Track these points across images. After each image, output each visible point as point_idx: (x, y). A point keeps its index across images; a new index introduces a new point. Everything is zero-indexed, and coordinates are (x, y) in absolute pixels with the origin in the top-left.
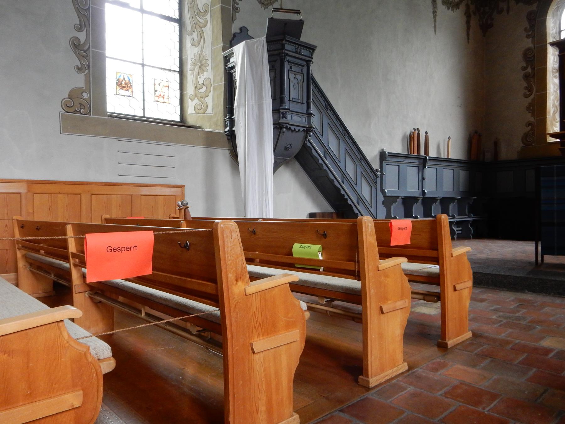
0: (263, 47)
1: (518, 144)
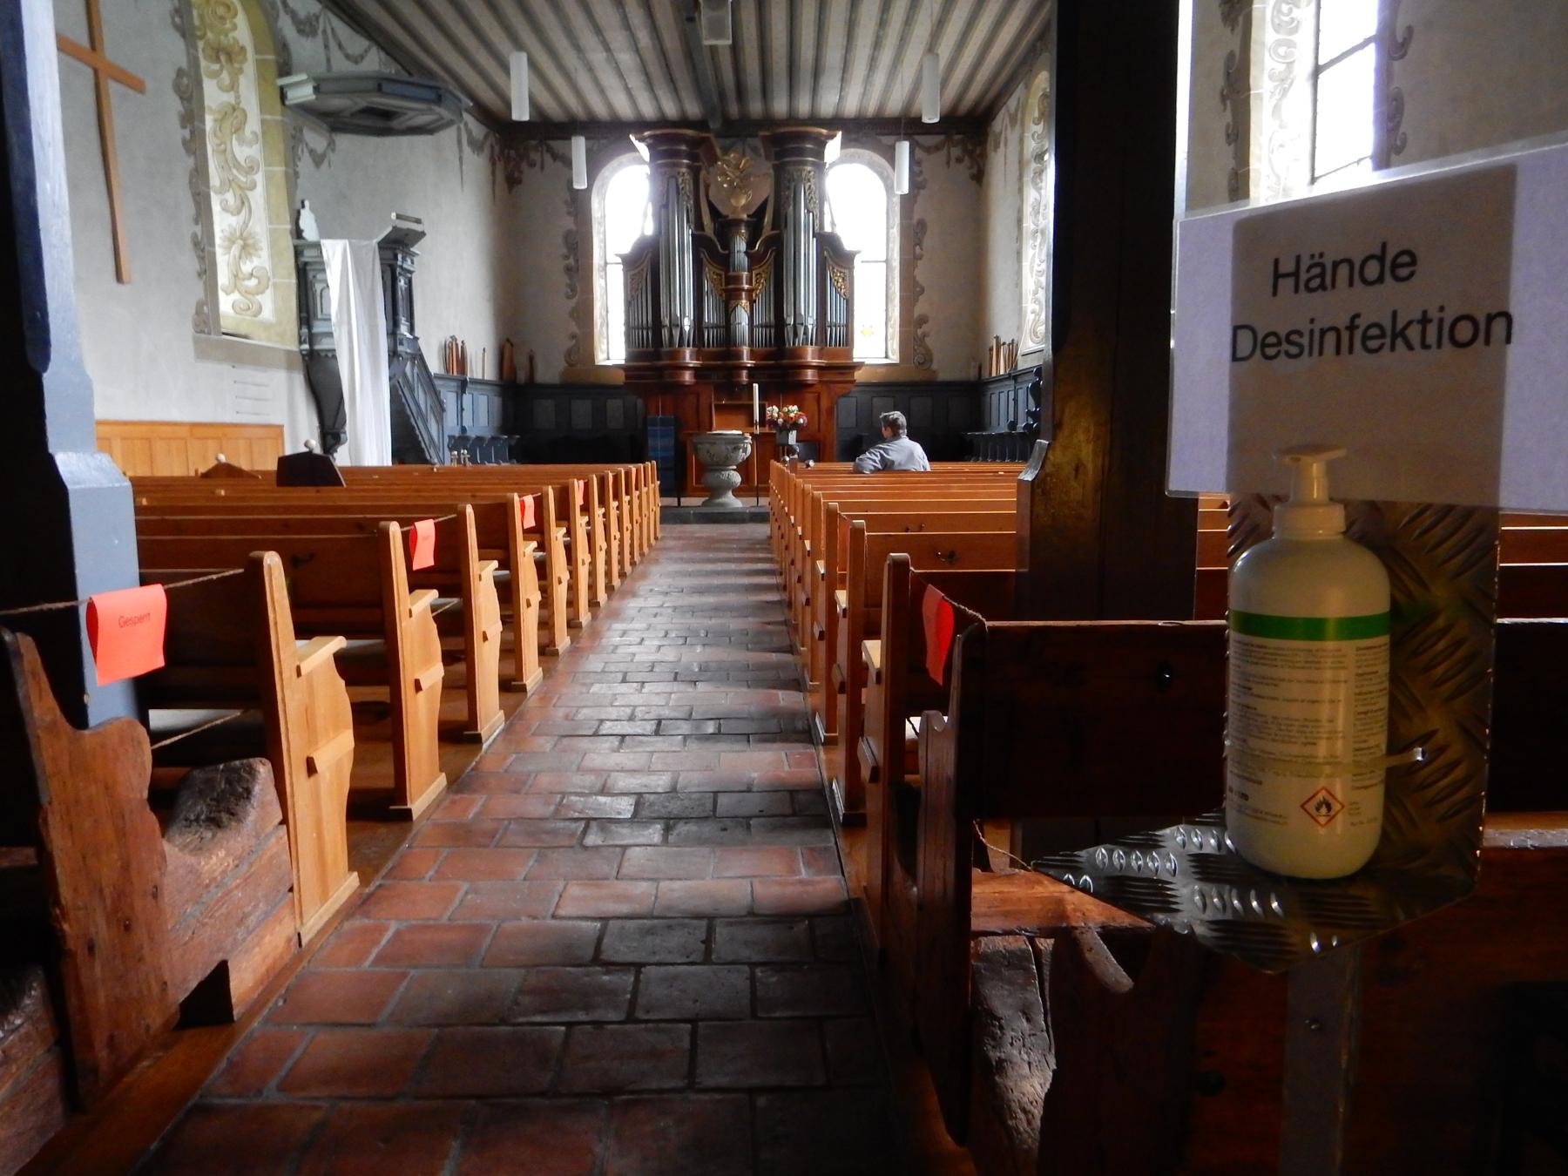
0: (374, 252)
1: (561, 365)
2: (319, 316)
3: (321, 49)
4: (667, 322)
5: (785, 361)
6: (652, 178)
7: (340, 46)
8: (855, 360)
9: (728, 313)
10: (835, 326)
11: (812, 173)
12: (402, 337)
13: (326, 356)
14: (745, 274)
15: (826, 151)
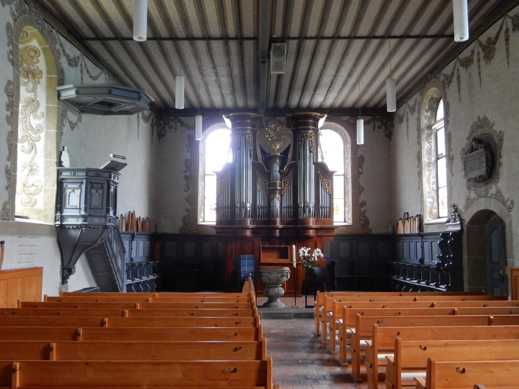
1: (180, 224)
2: (67, 207)
3: (79, 72)
4: (238, 205)
5: (299, 226)
6: (232, 135)
7: (88, 71)
8: (335, 224)
9: (269, 200)
10: (324, 208)
11: (313, 134)
12: (110, 218)
13: (69, 227)
14: (278, 182)
15: (319, 124)
